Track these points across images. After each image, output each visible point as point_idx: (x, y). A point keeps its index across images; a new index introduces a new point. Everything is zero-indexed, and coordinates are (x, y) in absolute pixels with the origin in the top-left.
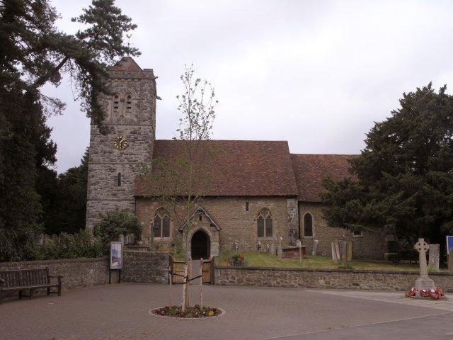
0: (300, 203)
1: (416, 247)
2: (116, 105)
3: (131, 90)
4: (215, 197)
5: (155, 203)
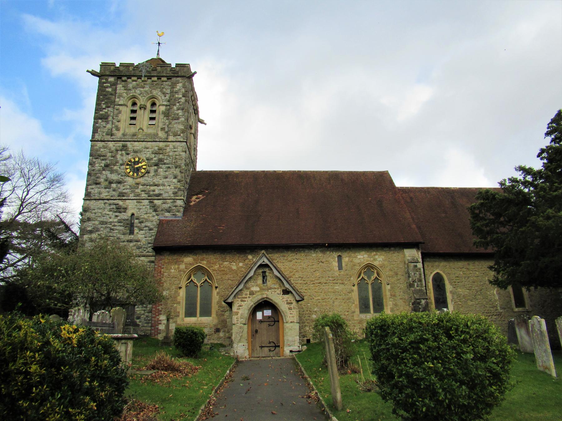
2: (153, 115)
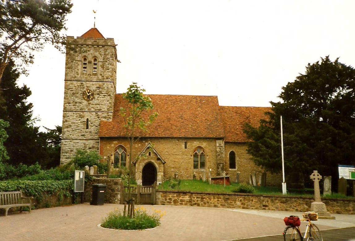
0: (226, 143)
1: (312, 177)
3: (97, 54)
4: (162, 138)
5: (115, 142)
